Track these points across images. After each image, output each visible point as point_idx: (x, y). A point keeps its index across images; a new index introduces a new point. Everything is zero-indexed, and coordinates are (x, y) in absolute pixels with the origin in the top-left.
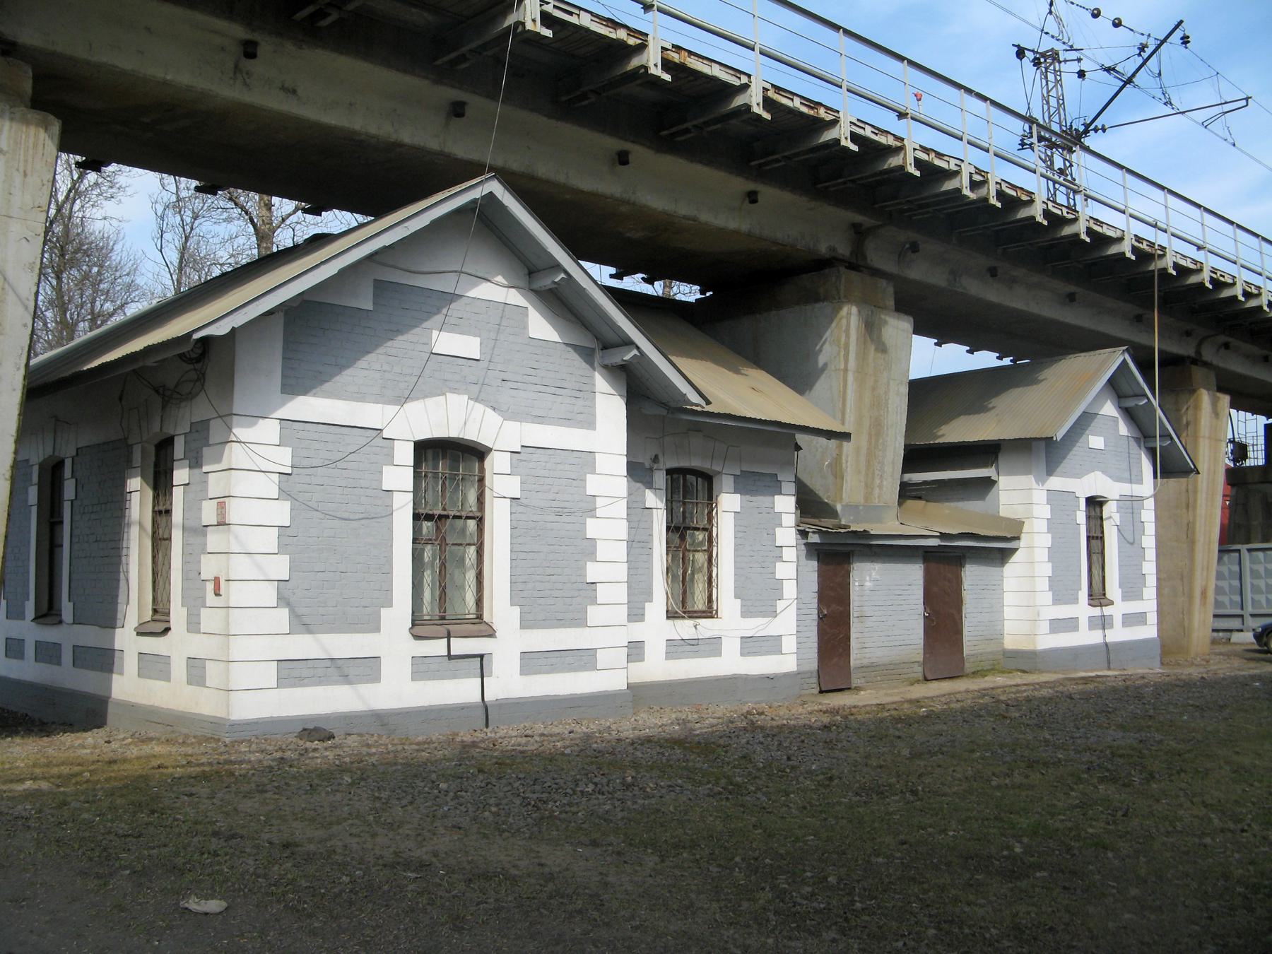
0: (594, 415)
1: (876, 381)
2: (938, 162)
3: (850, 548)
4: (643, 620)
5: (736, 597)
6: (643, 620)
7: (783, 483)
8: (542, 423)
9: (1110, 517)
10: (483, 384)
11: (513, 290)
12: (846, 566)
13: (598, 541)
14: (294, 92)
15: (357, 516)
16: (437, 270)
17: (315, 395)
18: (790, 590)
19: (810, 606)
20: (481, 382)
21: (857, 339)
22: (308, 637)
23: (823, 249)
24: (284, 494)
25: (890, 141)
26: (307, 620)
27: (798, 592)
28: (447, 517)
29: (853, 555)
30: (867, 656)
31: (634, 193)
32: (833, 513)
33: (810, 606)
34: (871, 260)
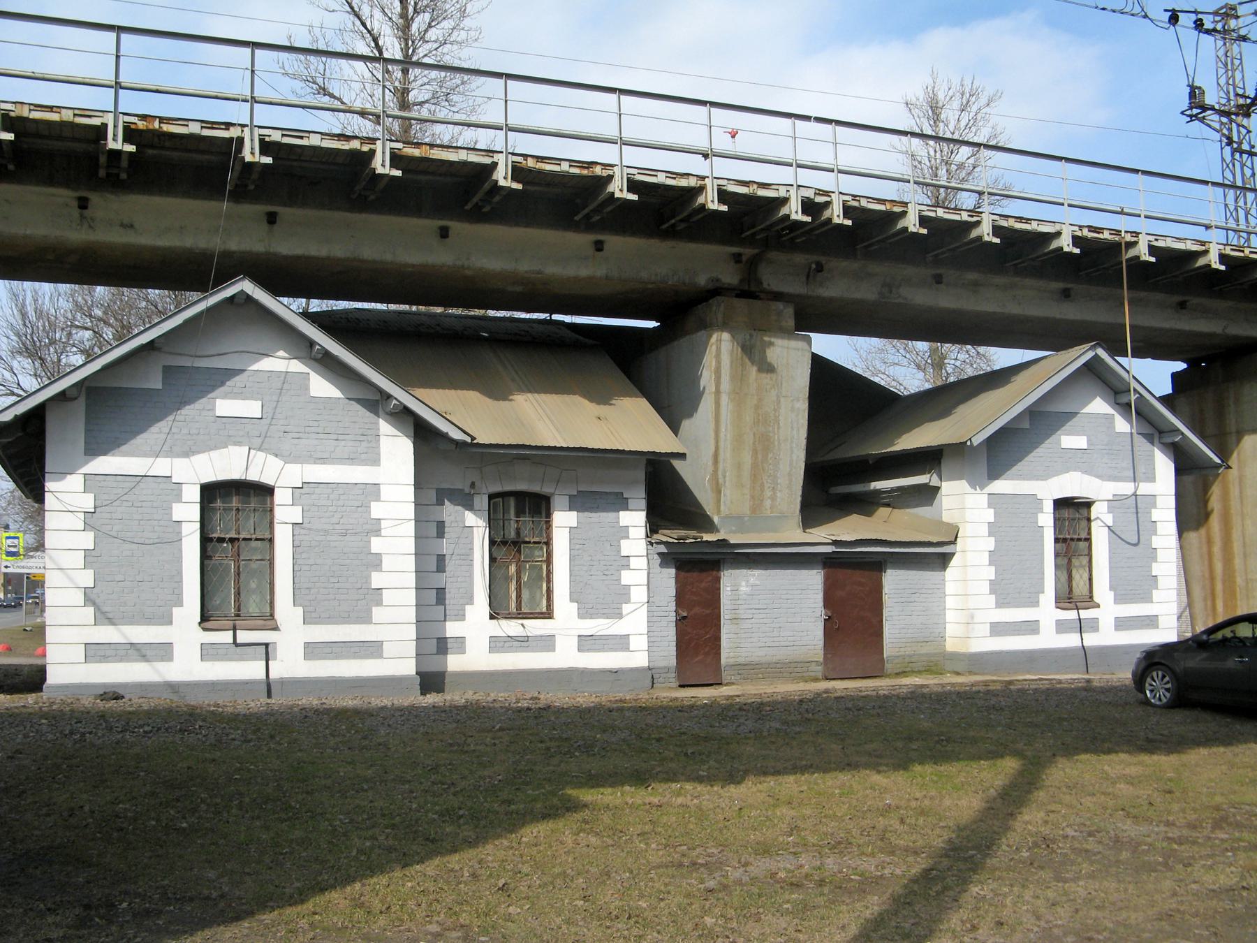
0: (379, 454)
1: (760, 400)
2: (762, 193)
3: (719, 557)
4: (464, 620)
5: (572, 600)
6: (464, 620)
7: (629, 500)
8: (324, 463)
9: (1098, 518)
10: (266, 437)
11: (295, 360)
12: (715, 573)
13: (383, 556)
14: (132, 226)
15: (151, 541)
16: (221, 352)
17: (113, 455)
18: (639, 594)
19: (668, 609)
20: (263, 435)
21: (732, 362)
22: (111, 628)
23: (702, 280)
24: (87, 526)
25: (693, 182)
26: (110, 615)
27: (649, 597)
28: (238, 539)
29: (724, 563)
30: (744, 655)
31: (468, 259)
32: (709, 526)
33: (668, 609)
34: (769, 285)
